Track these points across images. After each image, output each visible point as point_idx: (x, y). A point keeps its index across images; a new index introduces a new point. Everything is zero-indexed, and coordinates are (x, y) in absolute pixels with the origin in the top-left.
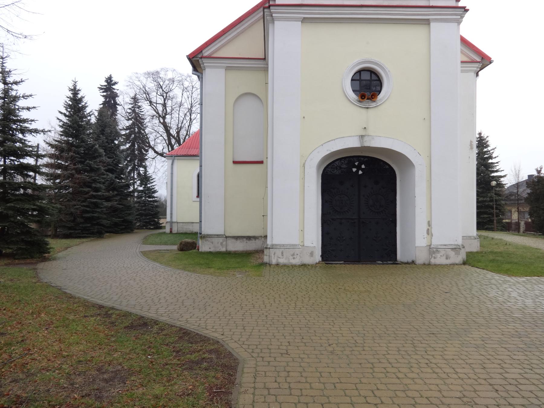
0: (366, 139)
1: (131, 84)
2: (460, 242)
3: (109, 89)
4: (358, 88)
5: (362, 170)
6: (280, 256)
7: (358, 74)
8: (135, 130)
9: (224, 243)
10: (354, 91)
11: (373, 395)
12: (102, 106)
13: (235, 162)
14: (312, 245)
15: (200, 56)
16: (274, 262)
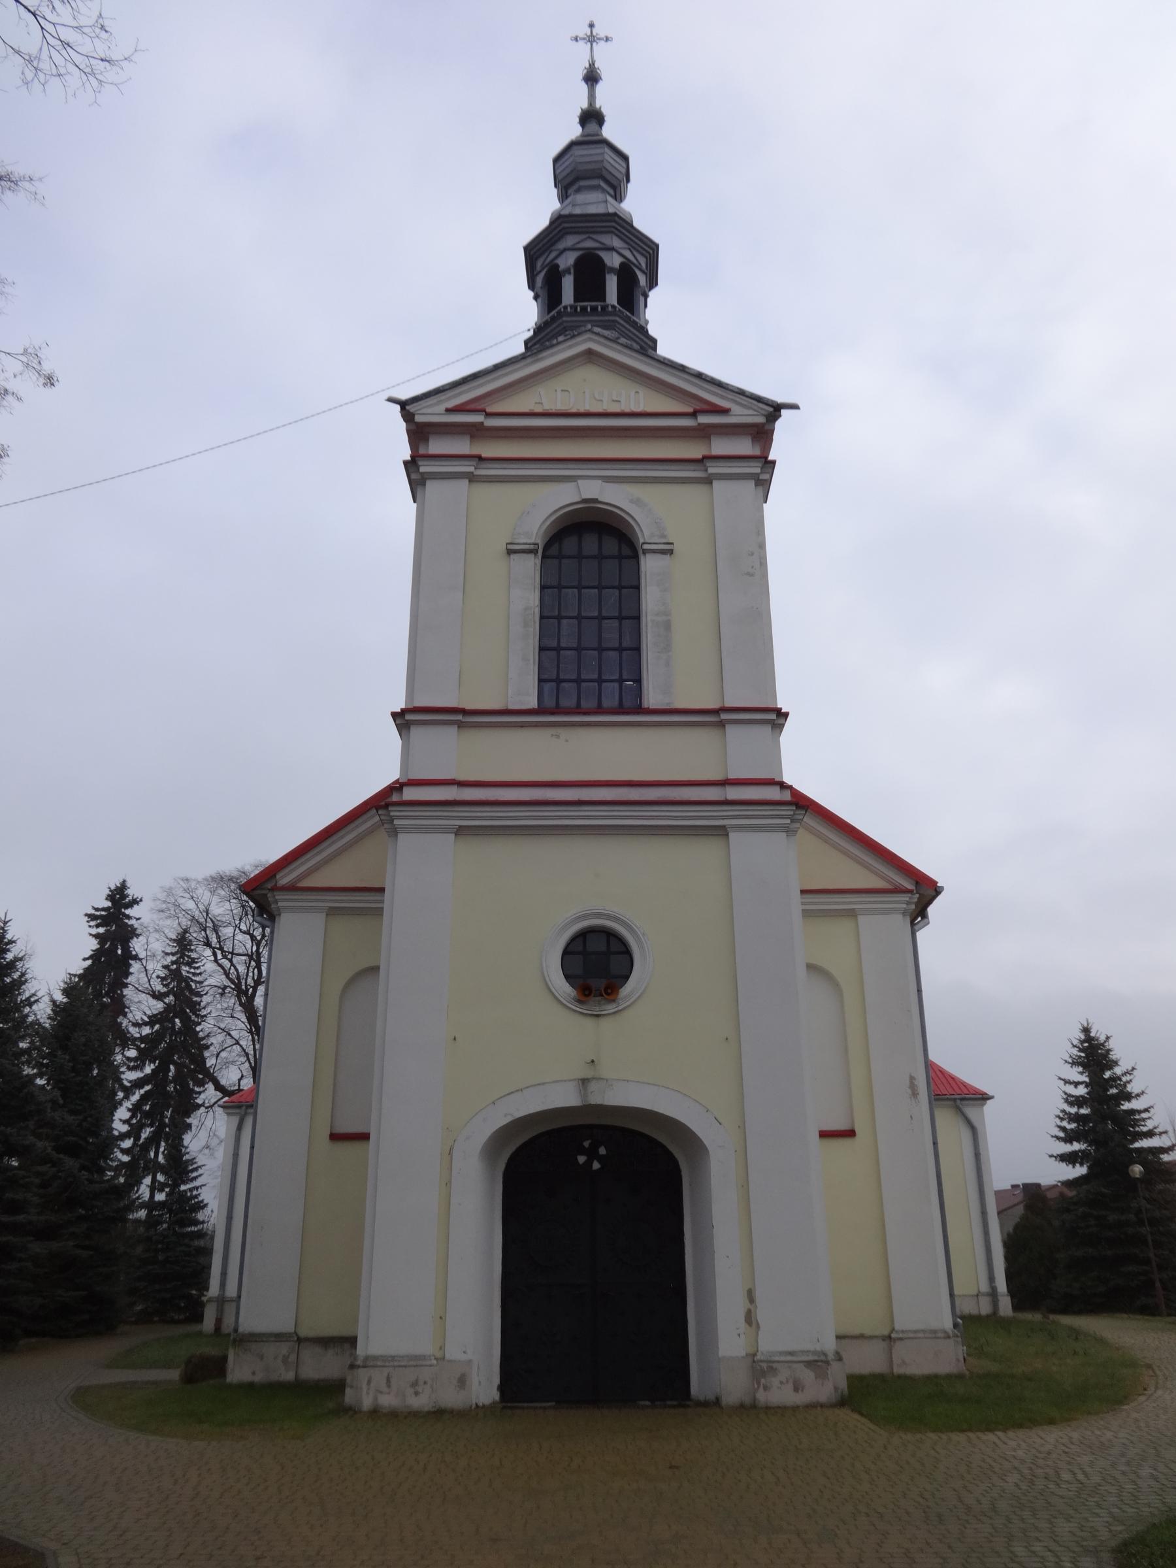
0: (593, 1086)
1: (170, 906)
2: (829, 1344)
3: (114, 920)
5: (601, 1159)
6: (384, 1388)
8: (174, 1024)
9: (293, 1357)
10: (567, 977)
12: (89, 962)
13: (335, 1137)
14: (463, 1357)
15: (269, 886)
16: (367, 1403)
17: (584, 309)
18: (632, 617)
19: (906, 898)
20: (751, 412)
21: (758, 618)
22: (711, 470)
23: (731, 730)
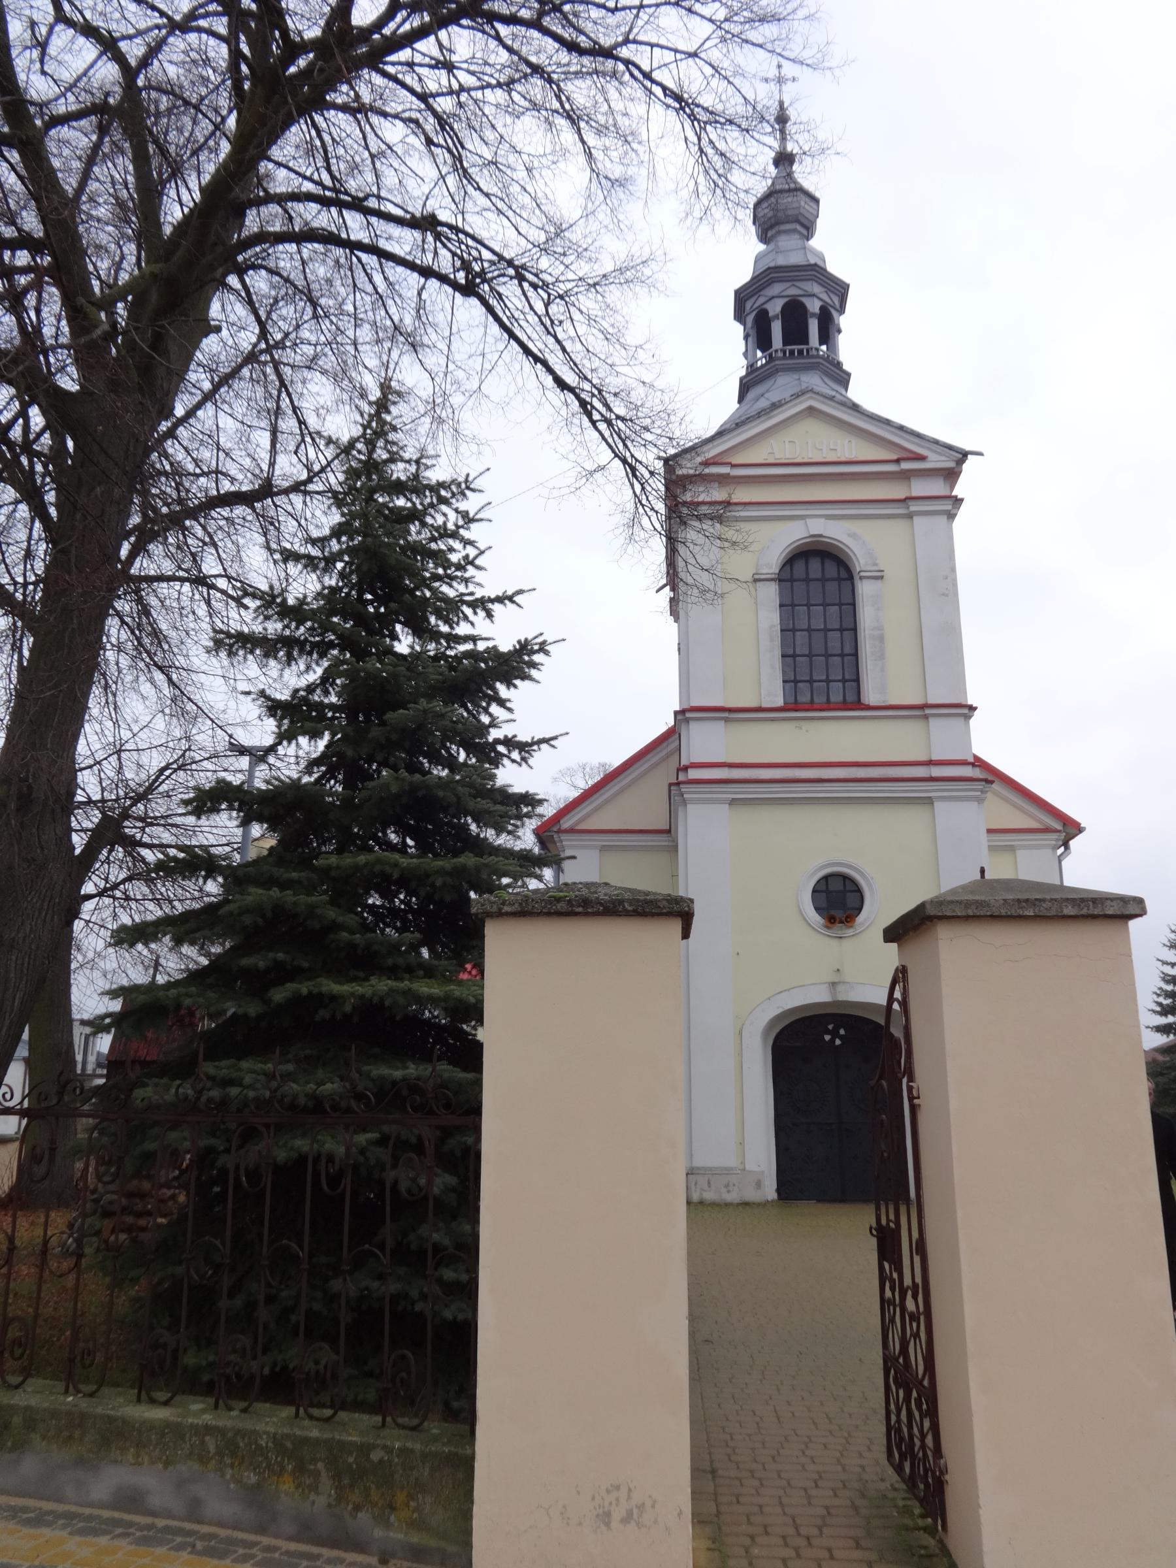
0: (840, 988)
4: (824, 905)
5: (841, 1037)
6: (706, 1187)
7: (823, 882)
10: (816, 909)
17: (792, 352)
18: (852, 629)
19: (1055, 836)
20: (943, 458)
21: (951, 631)
22: (912, 509)
23: (932, 721)
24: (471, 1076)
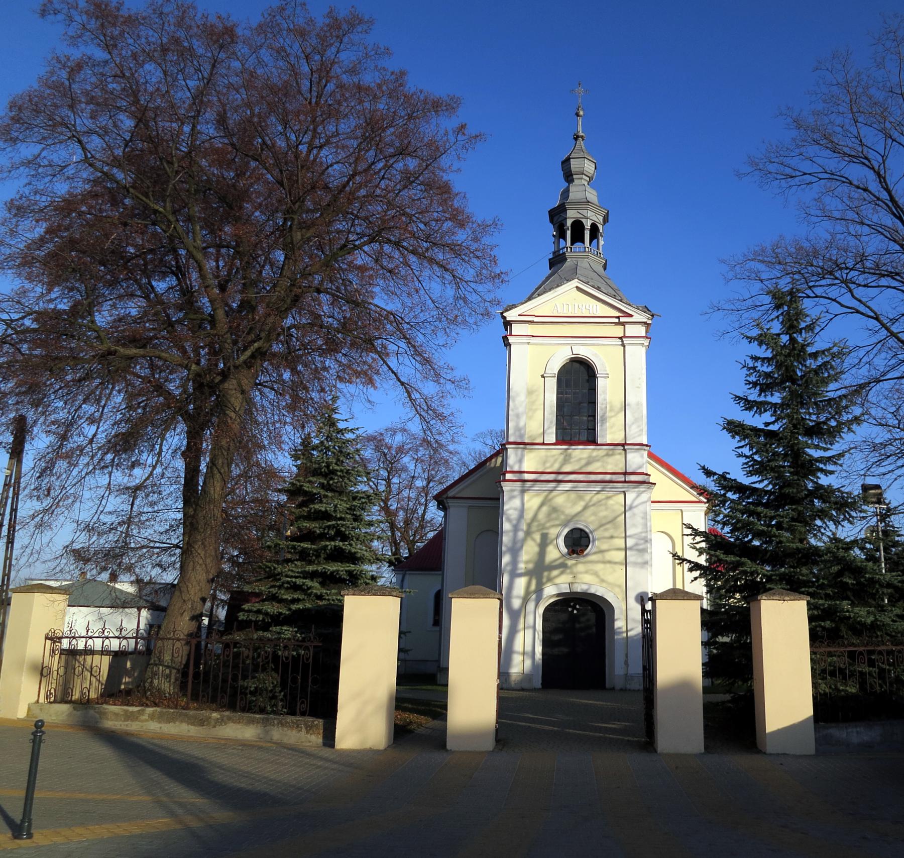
0: (576, 585)
5: (577, 610)
11: (868, 304)
24: (436, 723)
